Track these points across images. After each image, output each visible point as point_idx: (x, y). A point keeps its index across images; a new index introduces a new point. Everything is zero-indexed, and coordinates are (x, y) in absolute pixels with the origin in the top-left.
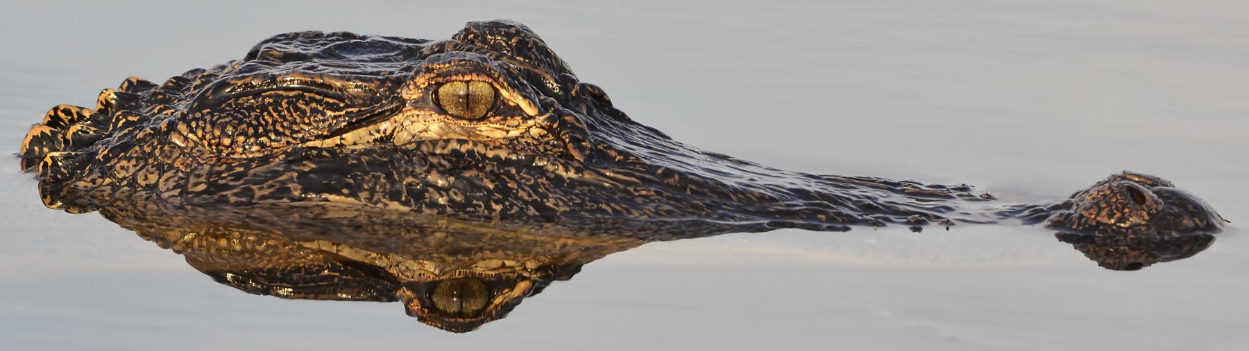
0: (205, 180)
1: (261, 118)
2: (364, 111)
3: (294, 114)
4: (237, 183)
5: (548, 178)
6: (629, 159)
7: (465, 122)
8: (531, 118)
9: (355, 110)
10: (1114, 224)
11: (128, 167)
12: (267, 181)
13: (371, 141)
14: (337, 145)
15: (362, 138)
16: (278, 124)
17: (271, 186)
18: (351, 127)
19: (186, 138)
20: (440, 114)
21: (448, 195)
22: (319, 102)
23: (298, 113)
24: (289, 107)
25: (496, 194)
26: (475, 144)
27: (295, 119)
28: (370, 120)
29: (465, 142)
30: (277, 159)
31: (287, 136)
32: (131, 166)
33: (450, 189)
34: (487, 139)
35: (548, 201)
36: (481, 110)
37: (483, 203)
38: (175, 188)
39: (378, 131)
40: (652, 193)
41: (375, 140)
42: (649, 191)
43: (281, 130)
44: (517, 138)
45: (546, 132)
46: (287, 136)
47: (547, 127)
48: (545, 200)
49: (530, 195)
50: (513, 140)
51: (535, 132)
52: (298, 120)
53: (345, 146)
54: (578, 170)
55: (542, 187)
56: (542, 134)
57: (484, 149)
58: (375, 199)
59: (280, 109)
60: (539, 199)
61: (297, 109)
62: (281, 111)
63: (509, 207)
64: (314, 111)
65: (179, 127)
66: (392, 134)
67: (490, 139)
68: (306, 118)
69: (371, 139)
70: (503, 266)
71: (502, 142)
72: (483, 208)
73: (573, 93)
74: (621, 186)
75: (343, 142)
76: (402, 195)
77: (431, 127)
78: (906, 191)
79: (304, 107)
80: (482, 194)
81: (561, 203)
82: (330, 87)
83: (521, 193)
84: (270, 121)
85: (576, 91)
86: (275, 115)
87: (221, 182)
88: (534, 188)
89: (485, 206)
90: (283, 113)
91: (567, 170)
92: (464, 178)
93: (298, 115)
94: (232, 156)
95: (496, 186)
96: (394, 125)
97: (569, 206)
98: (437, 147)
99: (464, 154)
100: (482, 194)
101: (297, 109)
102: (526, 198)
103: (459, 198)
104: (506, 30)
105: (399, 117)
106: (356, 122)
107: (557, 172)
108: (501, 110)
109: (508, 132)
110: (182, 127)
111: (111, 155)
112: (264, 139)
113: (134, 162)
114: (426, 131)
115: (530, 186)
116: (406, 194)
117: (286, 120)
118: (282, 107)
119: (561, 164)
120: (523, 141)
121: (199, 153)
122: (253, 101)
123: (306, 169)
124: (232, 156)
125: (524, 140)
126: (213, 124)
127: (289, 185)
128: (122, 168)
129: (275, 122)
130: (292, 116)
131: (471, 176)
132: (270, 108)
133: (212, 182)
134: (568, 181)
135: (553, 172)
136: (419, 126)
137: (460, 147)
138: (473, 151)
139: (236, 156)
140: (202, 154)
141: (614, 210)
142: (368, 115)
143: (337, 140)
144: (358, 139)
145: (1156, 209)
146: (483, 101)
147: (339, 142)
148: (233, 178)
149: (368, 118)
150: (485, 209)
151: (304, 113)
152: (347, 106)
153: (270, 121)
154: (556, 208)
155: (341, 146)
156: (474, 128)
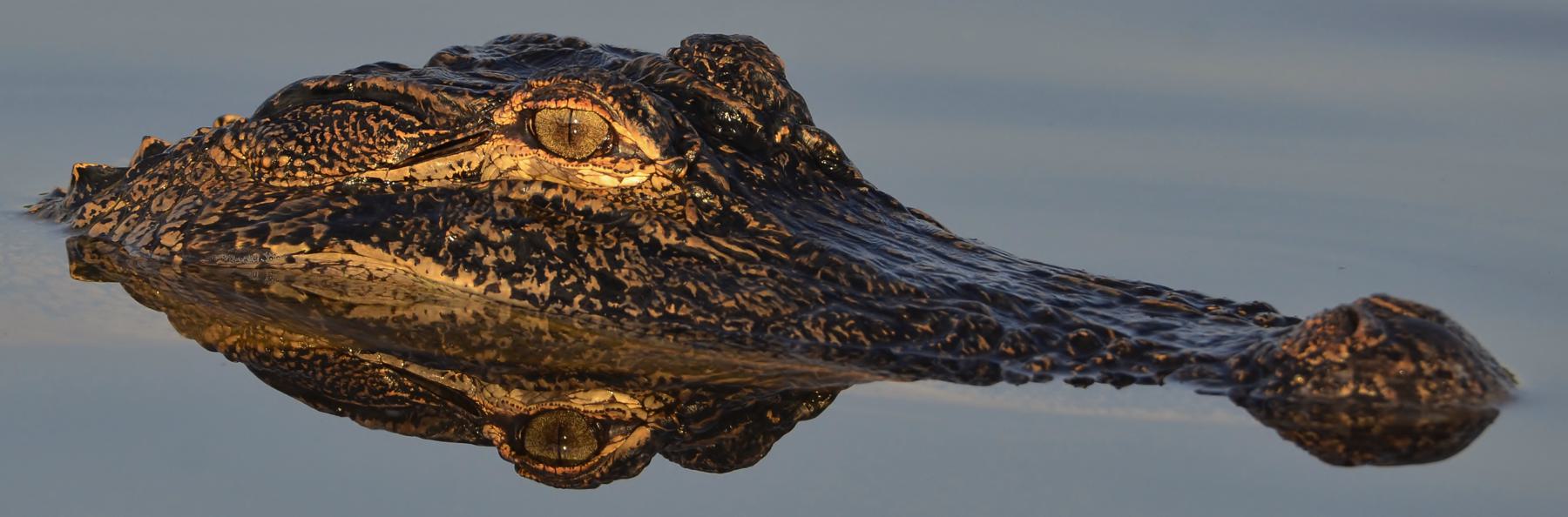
0: (220, 212)
1: (318, 135)
2: (442, 135)
3: (359, 132)
4: (257, 218)
5: (638, 242)
6: (765, 227)
7: (562, 161)
8: (653, 162)
9: (432, 132)
10: (1303, 359)
11: (147, 187)
12: (290, 218)
13: (450, 176)
14: (406, 179)
15: (439, 171)
16: (335, 144)
17: (294, 225)
18: (426, 155)
19: (228, 154)
20: (532, 147)
21: (497, 254)
22: (392, 119)
23: (364, 131)
24: (356, 123)
25: (557, 258)
26: (565, 190)
27: (358, 138)
28: (450, 149)
29: (555, 186)
30: (322, 191)
31: (342, 160)
32: (150, 186)
33: (502, 247)
34: (593, 187)
35: (620, 272)
36: (588, 145)
37: (536, 268)
38: (182, 218)
39: (460, 164)
40: (764, 273)
41: (456, 176)
42: (761, 269)
43: (337, 151)
44: (632, 188)
45: (670, 183)
46: (342, 160)
47: (671, 176)
48: (616, 271)
49: (599, 262)
50: (627, 189)
51: (658, 182)
52: (362, 139)
53: (418, 181)
54: (682, 235)
55: (623, 252)
56: (665, 185)
57: (575, 198)
58: (407, 252)
59: (345, 123)
60: (609, 269)
61: (365, 126)
62: (346, 127)
63: (564, 276)
64: (385, 129)
65: (547, 239)
66: (479, 169)
67: (597, 187)
68: (371, 139)
69: (450, 174)
70: (613, 400)
71: (611, 192)
72: (533, 275)
73: (778, 139)
74: (730, 260)
75: (413, 174)
76: (441, 248)
77: (521, 164)
78: (774, 226)
79: (372, 123)
80: (538, 256)
81: (635, 275)
82: (412, 99)
83: (590, 259)
84: (328, 139)
85: (783, 136)
86: (337, 131)
87: (241, 215)
88: (610, 254)
89: (537, 273)
90: (347, 130)
91: (667, 235)
92: (525, 233)
93: (363, 134)
94: (271, 183)
95: (560, 247)
96: (482, 157)
97: (645, 281)
98: (1310, 381)
99: (546, 202)
100: (538, 256)
101: (365, 126)
102: (593, 265)
103: (511, 258)
104: (721, 47)
105: (486, 147)
106: (432, 149)
107: (655, 235)
108: (610, 147)
109: (621, 179)
110: (227, 141)
111: (138, 171)
112: (313, 162)
113: (155, 181)
114: (516, 168)
115: (606, 251)
116: (446, 249)
117: (347, 139)
118: (348, 122)
119: (662, 225)
120: (637, 192)
121: (238, 176)
122: (320, 111)
123: (345, 207)
124: (271, 183)
125: (640, 191)
126: (260, 138)
127: (313, 226)
128: (140, 188)
129: (333, 140)
130: (355, 134)
131: (533, 230)
132: (335, 122)
133: (229, 214)
134: (664, 248)
135: (650, 235)
136: (507, 162)
137: (1383, 387)
138: (560, 199)
139: (276, 183)
140: (240, 178)
141: (700, 291)
142: (447, 141)
143: (406, 171)
144: (438, 171)
145: (1364, 344)
146: (590, 134)
147: (408, 174)
148: (255, 211)
149: (446, 145)
150: (535, 276)
151: (370, 130)
152: (425, 127)
153: (328, 139)
154: (626, 282)
155: (412, 180)
156: (575, 170)
